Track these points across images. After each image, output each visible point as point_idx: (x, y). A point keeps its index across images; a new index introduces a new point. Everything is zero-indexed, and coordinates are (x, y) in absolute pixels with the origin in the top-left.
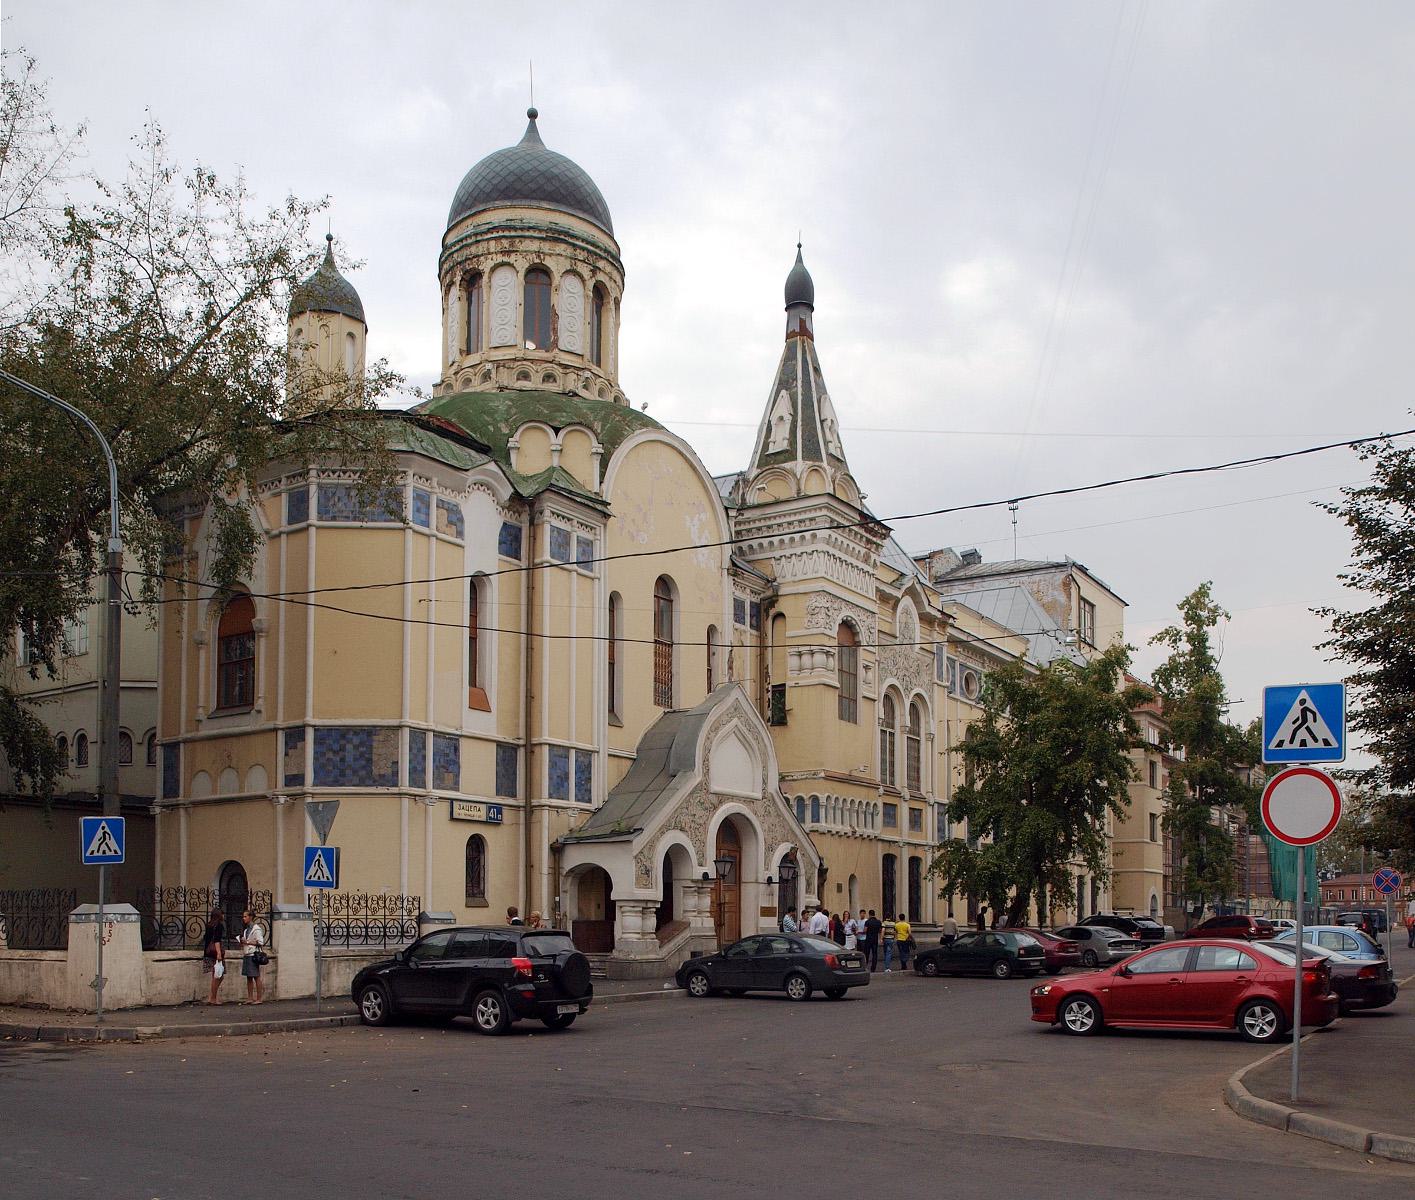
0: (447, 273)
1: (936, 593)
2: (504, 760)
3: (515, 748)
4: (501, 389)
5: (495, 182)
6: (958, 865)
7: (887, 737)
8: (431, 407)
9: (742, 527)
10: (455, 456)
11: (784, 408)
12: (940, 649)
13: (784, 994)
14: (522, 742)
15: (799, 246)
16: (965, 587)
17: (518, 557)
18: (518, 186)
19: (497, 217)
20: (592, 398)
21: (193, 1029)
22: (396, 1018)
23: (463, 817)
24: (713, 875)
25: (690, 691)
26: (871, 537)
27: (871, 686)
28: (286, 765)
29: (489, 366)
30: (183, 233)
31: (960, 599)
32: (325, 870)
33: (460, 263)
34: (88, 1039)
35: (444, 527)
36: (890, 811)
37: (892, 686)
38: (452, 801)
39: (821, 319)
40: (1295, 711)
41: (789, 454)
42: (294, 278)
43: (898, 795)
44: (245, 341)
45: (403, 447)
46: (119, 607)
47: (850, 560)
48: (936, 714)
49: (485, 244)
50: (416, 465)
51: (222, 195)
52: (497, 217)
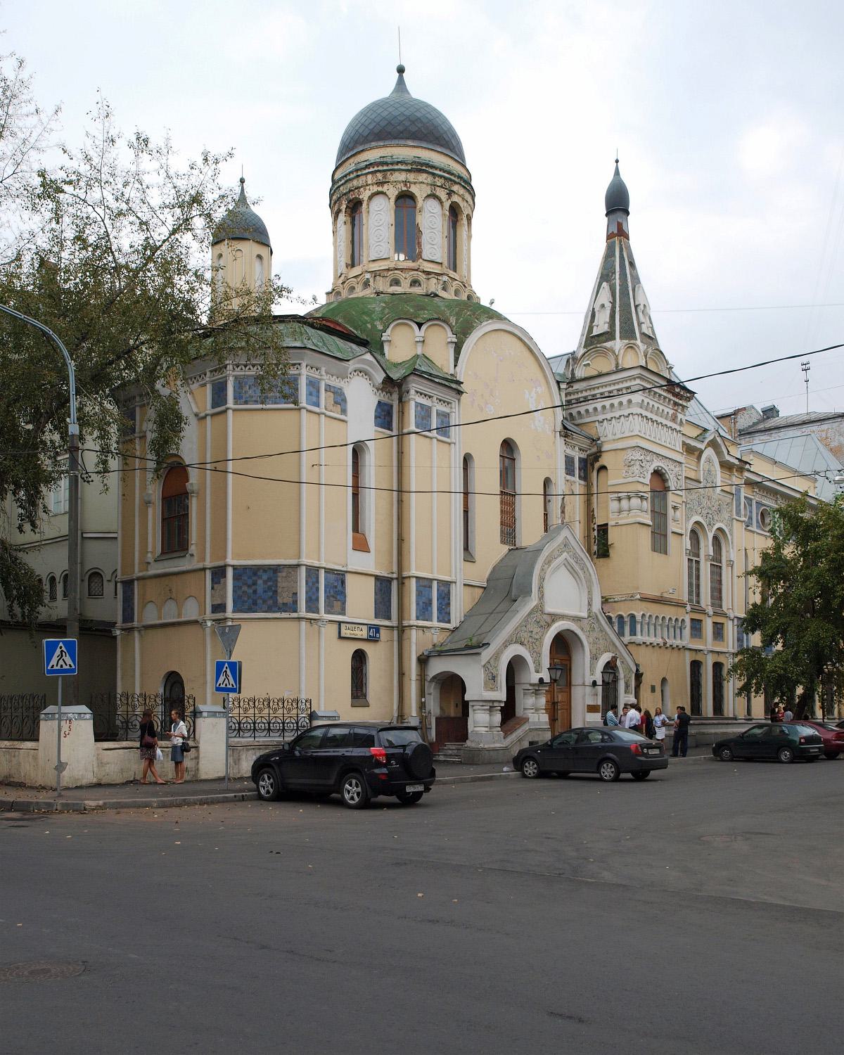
0: (335, 203)
1: (734, 443)
2: (381, 590)
4: (378, 294)
5: (371, 127)
6: (753, 667)
7: (694, 566)
8: (323, 311)
9: (572, 397)
10: (339, 350)
11: (605, 297)
12: (738, 491)
13: (597, 775)
14: (395, 576)
15: (617, 161)
16: (764, 437)
17: (390, 428)
18: (389, 129)
19: (373, 155)
21: (126, 803)
22: (284, 795)
24: (547, 680)
25: (530, 531)
26: (677, 400)
27: (679, 523)
28: (212, 596)
29: (368, 276)
30: (126, 184)
31: (755, 448)
32: (232, 681)
33: (345, 194)
34: (49, 809)
35: (331, 407)
36: (696, 626)
37: (697, 523)
38: (340, 623)
39: (634, 223)
41: (609, 336)
42: (209, 215)
43: (703, 612)
44: (172, 266)
45: (298, 344)
46: (77, 476)
47: (660, 420)
48: (735, 544)
49: (363, 178)
50: (309, 358)
51: (154, 152)
52: (373, 155)
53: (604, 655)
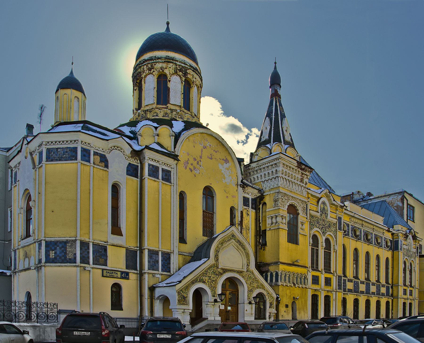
23: (109, 276)
27: (305, 230)
38: (103, 270)
41: (268, 142)
53: (256, 290)
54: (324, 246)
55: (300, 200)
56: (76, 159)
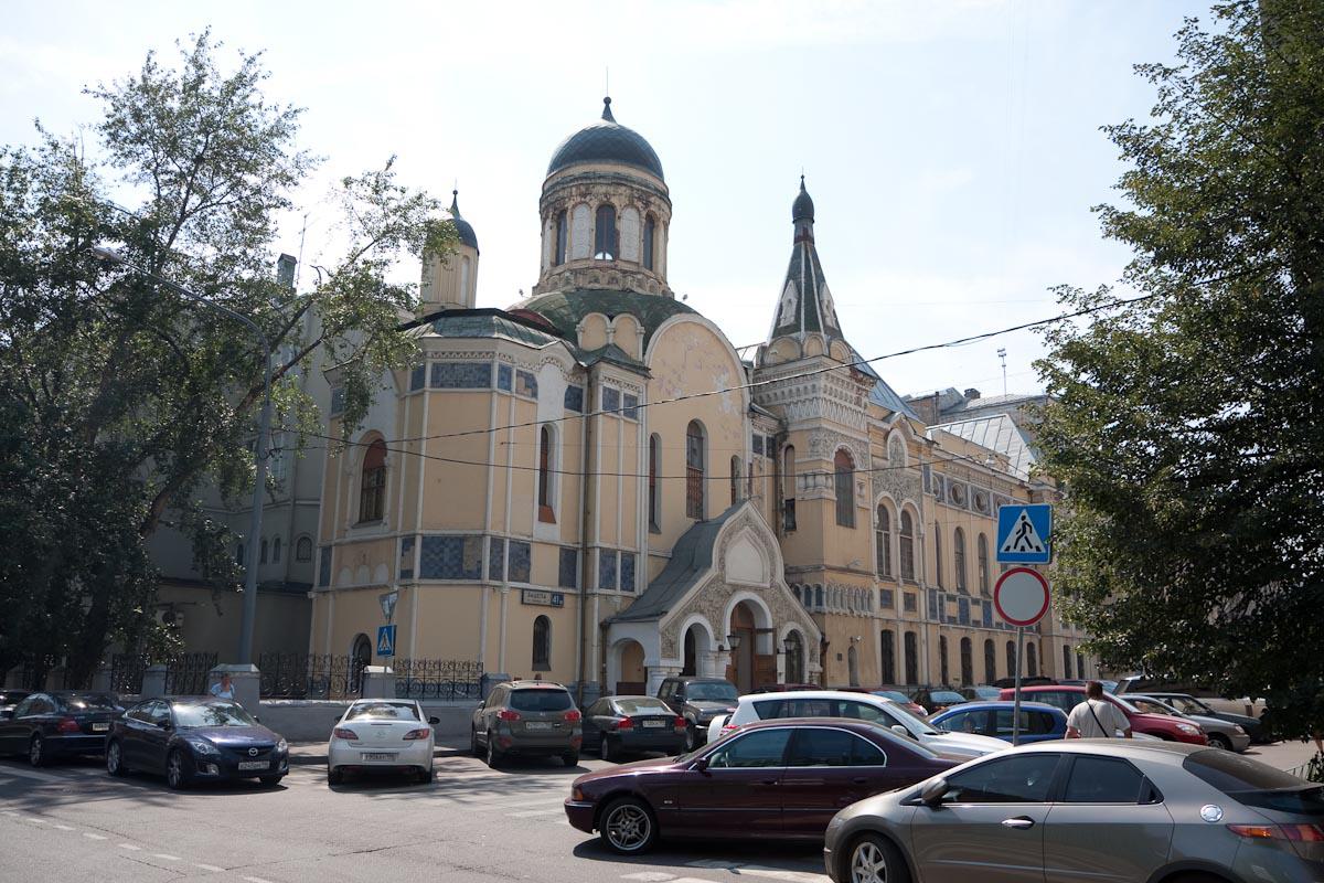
3: (575, 552)
4: (578, 289)
14: (580, 546)
17: (579, 410)
20: (644, 293)
27: (867, 498)
28: (402, 562)
33: (552, 203)
38: (523, 590)
39: (819, 230)
40: (1018, 525)
41: (795, 327)
54: (900, 527)
55: (856, 440)
56: (489, 385)
